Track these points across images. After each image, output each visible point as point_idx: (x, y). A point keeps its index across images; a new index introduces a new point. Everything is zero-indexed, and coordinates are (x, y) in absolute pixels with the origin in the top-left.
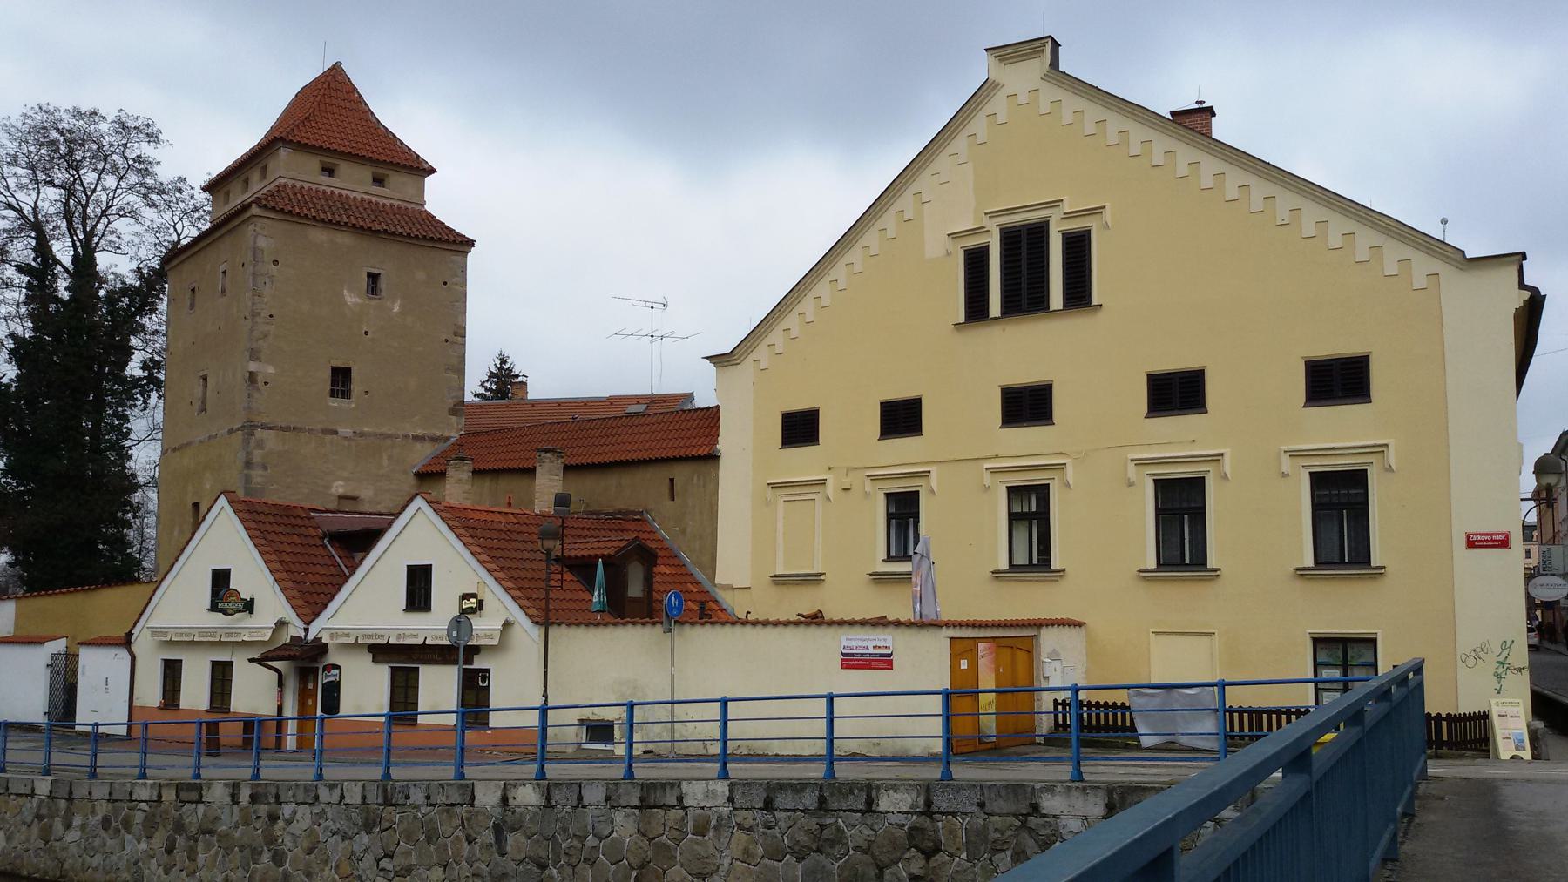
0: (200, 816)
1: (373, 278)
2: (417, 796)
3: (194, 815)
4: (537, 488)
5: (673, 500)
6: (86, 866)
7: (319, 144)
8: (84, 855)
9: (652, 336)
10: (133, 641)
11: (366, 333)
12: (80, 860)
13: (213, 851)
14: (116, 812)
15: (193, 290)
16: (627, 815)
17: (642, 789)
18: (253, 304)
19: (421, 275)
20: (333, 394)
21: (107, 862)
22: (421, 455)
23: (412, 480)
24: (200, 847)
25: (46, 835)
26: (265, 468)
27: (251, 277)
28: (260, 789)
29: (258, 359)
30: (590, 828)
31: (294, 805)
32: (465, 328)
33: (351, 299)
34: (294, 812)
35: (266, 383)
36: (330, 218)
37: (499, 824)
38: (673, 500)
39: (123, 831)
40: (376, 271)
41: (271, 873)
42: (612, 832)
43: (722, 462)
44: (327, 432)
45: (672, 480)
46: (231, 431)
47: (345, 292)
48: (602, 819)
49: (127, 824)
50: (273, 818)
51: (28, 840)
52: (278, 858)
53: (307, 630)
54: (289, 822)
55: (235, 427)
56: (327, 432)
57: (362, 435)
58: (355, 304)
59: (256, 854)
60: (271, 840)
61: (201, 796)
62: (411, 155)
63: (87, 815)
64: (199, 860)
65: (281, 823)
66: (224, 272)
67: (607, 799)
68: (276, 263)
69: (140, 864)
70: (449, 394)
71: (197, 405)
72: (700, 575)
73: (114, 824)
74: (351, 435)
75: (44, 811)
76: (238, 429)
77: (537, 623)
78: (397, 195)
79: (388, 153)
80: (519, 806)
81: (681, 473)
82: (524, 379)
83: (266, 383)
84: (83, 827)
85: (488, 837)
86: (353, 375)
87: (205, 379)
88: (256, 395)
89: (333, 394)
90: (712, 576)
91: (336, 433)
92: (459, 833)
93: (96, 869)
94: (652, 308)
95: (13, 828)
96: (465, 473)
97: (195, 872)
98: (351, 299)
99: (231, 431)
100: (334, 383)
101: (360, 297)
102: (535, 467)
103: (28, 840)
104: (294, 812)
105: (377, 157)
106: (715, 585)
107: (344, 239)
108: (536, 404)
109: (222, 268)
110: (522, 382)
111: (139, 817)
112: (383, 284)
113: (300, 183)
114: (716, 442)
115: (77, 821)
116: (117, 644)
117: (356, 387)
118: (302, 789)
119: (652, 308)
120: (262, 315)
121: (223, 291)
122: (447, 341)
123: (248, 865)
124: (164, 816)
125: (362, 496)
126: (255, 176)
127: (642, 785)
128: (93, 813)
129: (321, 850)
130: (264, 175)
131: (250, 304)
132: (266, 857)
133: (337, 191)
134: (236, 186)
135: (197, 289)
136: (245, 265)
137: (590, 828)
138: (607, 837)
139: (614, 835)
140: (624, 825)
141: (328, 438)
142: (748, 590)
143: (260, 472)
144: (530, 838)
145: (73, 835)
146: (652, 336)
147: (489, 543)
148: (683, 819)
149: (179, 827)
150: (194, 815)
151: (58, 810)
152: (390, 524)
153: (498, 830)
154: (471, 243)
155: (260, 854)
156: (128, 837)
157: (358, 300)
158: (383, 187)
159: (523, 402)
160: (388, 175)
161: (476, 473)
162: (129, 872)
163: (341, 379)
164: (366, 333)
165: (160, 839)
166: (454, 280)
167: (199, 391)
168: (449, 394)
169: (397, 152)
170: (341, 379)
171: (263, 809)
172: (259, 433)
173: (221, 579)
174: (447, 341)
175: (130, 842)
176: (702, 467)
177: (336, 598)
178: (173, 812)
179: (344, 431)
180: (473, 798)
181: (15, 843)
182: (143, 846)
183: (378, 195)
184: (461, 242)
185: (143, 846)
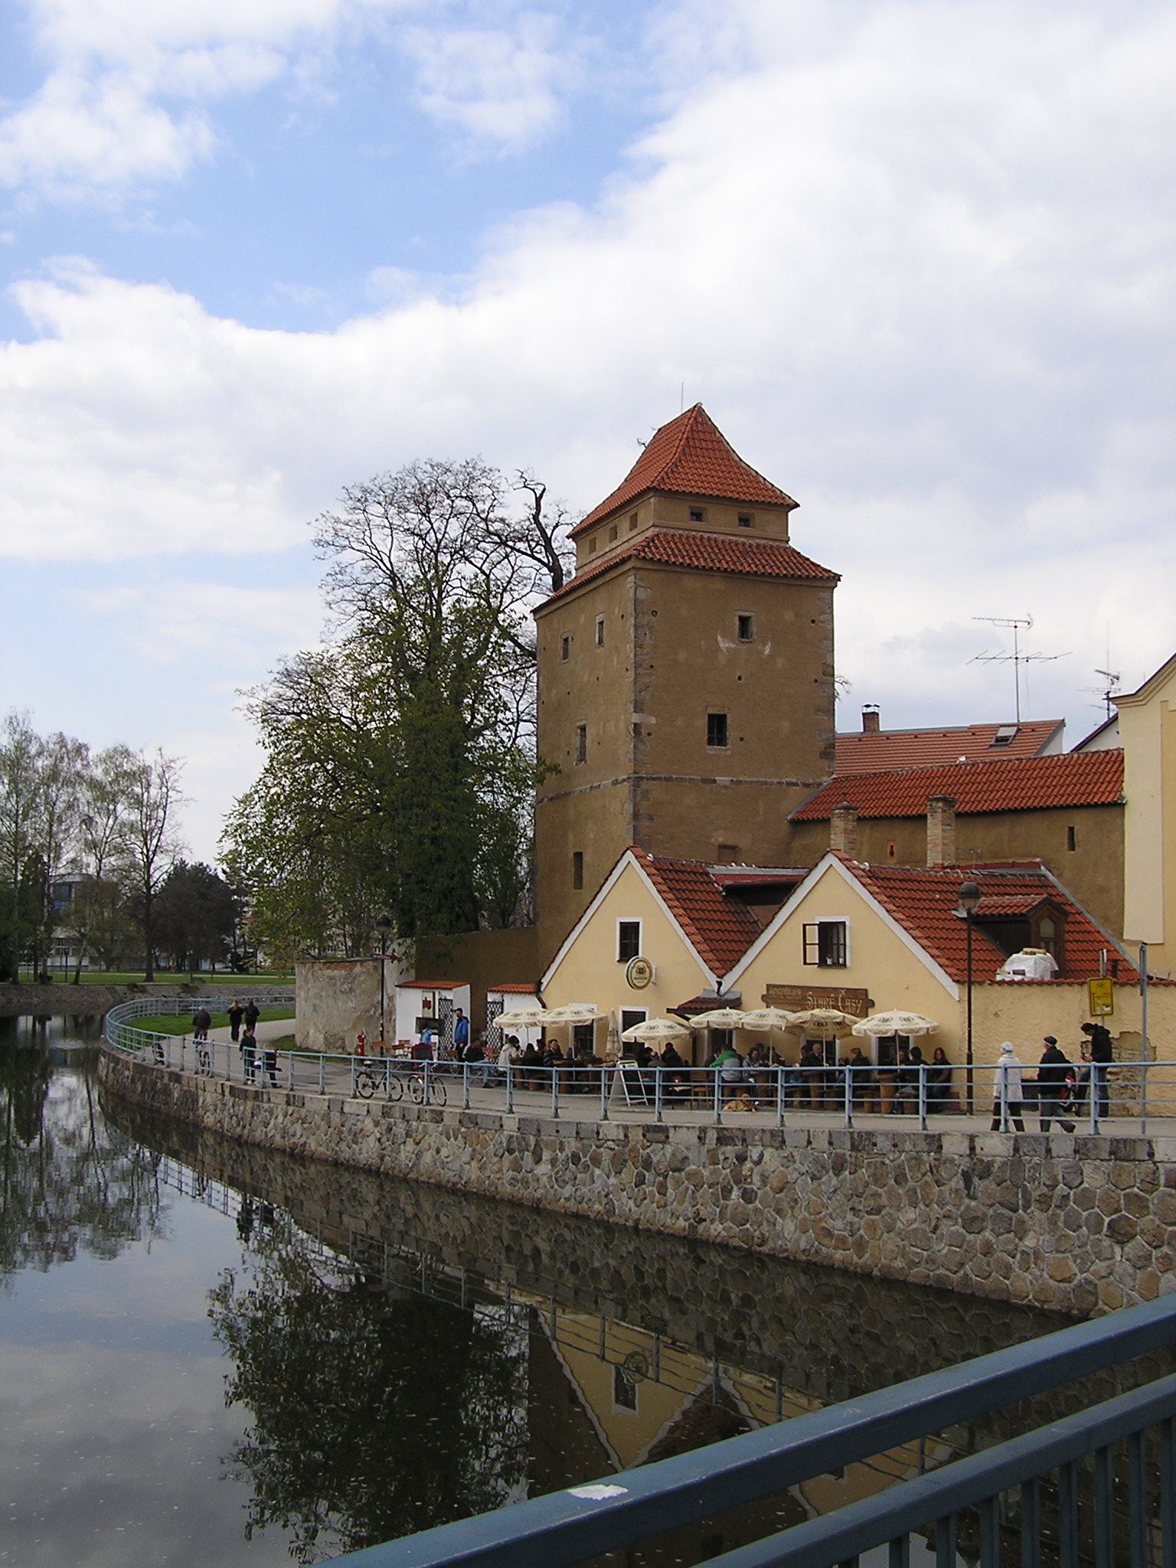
0: (668, 1156)
1: (744, 621)
2: (883, 1144)
3: (661, 1155)
4: (929, 838)
5: (1073, 849)
6: (558, 1197)
7: (688, 490)
8: (556, 1186)
9: (1017, 658)
10: (542, 990)
11: (740, 678)
12: (552, 1191)
13: (682, 1188)
14: (585, 1149)
15: (566, 640)
16: (1097, 1168)
17: (1111, 1144)
18: (635, 655)
19: (789, 616)
20: (710, 742)
21: (578, 1193)
22: (792, 804)
23: (785, 826)
24: (670, 1183)
25: (517, 1167)
26: (651, 819)
27: (632, 629)
28: (726, 1132)
29: (642, 711)
30: (1060, 1178)
31: (761, 1148)
32: (833, 667)
33: (724, 644)
34: (762, 1156)
35: (649, 734)
36: (703, 564)
37: (967, 1172)
38: (1073, 849)
39: (591, 1166)
40: (747, 614)
41: (740, 1208)
42: (1082, 1182)
43: (1127, 810)
44: (705, 781)
45: (1071, 829)
46: (616, 783)
47: (719, 638)
48: (1070, 1170)
49: (596, 1161)
50: (742, 1159)
51: (500, 1170)
52: (748, 1196)
53: (720, 984)
54: (758, 1162)
55: (620, 778)
56: (705, 781)
57: (739, 782)
58: (729, 649)
59: (727, 1192)
60: (739, 1179)
61: (667, 1137)
62: (764, 484)
63: (556, 1150)
64: (668, 1194)
65: (748, 1165)
66: (601, 623)
67: (1076, 1152)
68: (654, 613)
69: (611, 1196)
70: (820, 736)
71: (575, 754)
72: (1106, 933)
73: (583, 1160)
74: (728, 784)
75: (515, 1145)
76: (624, 780)
77: (957, 982)
78: (764, 534)
79: (753, 491)
80: (987, 1156)
81: (1082, 822)
82: (876, 710)
83: (649, 734)
84: (553, 1162)
85: (957, 1182)
86: (729, 721)
87: (583, 729)
88: (641, 746)
89: (710, 742)
90: (1120, 934)
91: (715, 781)
92: (929, 1178)
93: (567, 1199)
94: (1016, 627)
95: (485, 1158)
96: (850, 823)
97: (666, 1205)
98: (724, 644)
99: (616, 783)
100: (710, 731)
101: (734, 643)
102: (926, 816)
103: (500, 1170)
104: (762, 1156)
105: (743, 497)
106: (1123, 941)
107: (718, 585)
108: (888, 736)
109: (598, 619)
110: (873, 713)
111: (606, 1155)
112: (754, 628)
113: (672, 530)
114: (1120, 781)
115: (546, 1155)
116: (526, 992)
117: (731, 734)
118: (769, 1135)
119: (1016, 627)
120: (645, 666)
121: (601, 642)
122: (816, 681)
123: (718, 1200)
124: (633, 1155)
125: (741, 846)
126: (624, 524)
127: (1111, 1140)
128: (562, 1150)
129: (789, 1190)
130: (634, 525)
131: (632, 655)
132: (735, 1194)
133: (706, 536)
134: (602, 534)
135: (570, 639)
136: (625, 618)
137: (1060, 1178)
138: (1077, 1187)
139: (1085, 1185)
140: (1094, 1177)
141: (708, 787)
142: (1162, 947)
143: (647, 823)
144: (999, 1185)
145: (543, 1169)
146: (1017, 658)
147: (903, 903)
148: (1154, 1172)
149: (647, 1164)
150: (661, 1155)
151: (527, 1145)
152: (801, 880)
153: (967, 1177)
154: (838, 577)
155: (730, 1192)
156: (597, 1172)
157: (732, 646)
158: (748, 526)
159: (875, 734)
160: (753, 514)
161: (860, 819)
162: (600, 1203)
163: (717, 729)
164: (740, 678)
165: (629, 1173)
166: (822, 618)
167: (576, 741)
168: (820, 736)
169: (761, 489)
170: (717, 729)
171: (730, 1150)
172: (644, 785)
173: (629, 934)
174: (816, 681)
175: (599, 1176)
176: (1114, 811)
177: (748, 953)
178: (641, 1151)
179: (723, 779)
180: (940, 1147)
181: (488, 1173)
182: (613, 1180)
183: (744, 536)
184: (828, 578)
185: (613, 1180)
